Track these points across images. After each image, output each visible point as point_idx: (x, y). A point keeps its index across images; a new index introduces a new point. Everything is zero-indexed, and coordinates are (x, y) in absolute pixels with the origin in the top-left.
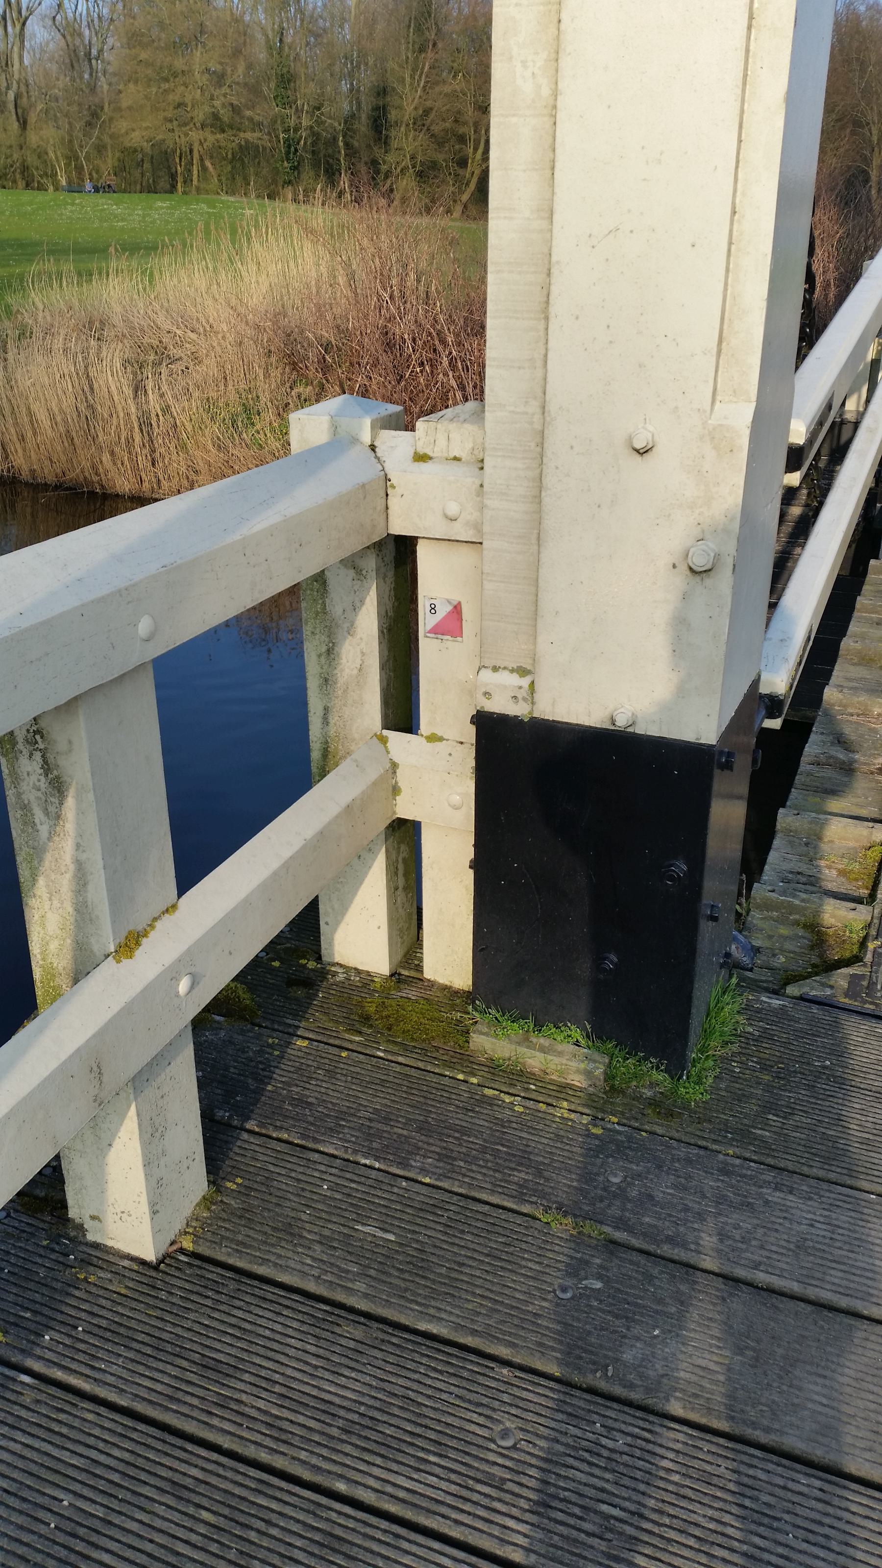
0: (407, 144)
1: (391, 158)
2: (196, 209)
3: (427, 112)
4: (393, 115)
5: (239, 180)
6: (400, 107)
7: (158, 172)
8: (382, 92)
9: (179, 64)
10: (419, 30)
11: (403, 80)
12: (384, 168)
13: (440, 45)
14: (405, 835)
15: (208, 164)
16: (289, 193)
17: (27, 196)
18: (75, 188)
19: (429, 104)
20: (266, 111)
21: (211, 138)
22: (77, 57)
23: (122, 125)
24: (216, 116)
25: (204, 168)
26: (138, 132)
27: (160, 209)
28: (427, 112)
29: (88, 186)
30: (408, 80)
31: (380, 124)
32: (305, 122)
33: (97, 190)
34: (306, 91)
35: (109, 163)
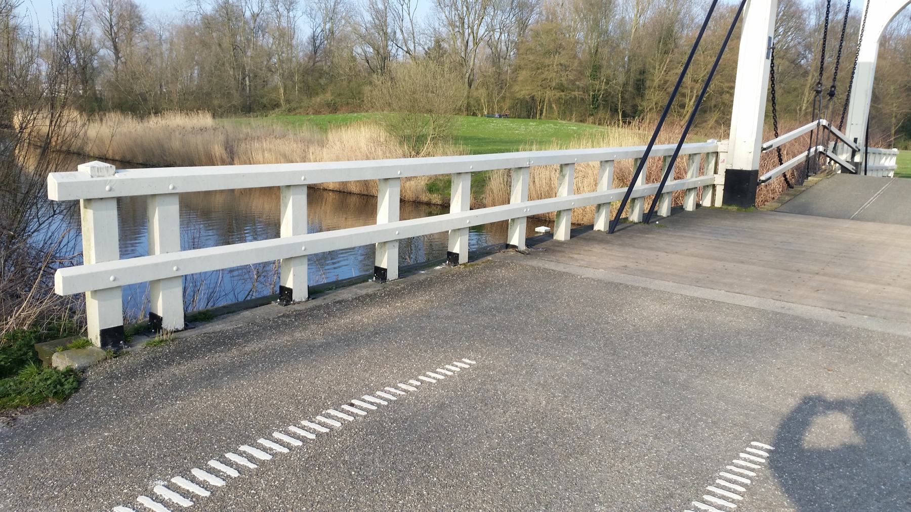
0: (654, 98)
1: (644, 104)
2: (549, 126)
3: (666, 82)
4: (648, 83)
5: (568, 113)
6: (653, 81)
7: (528, 109)
8: (643, 72)
9: (547, 61)
10: (665, 44)
11: (655, 68)
12: (640, 108)
13: (676, 50)
14: (714, 186)
15: (554, 106)
16: (591, 119)
17: (471, 118)
18: (490, 115)
19: (667, 78)
20: (586, 81)
21: (558, 94)
22: (496, 58)
23: (516, 88)
24: (562, 85)
25: (551, 107)
26: (523, 91)
27: (532, 126)
28: (666, 82)
29: (497, 115)
30: (657, 67)
31: (640, 86)
32: (603, 87)
33: (500, 116)
34: (605, 72)
35: (506, 105)
